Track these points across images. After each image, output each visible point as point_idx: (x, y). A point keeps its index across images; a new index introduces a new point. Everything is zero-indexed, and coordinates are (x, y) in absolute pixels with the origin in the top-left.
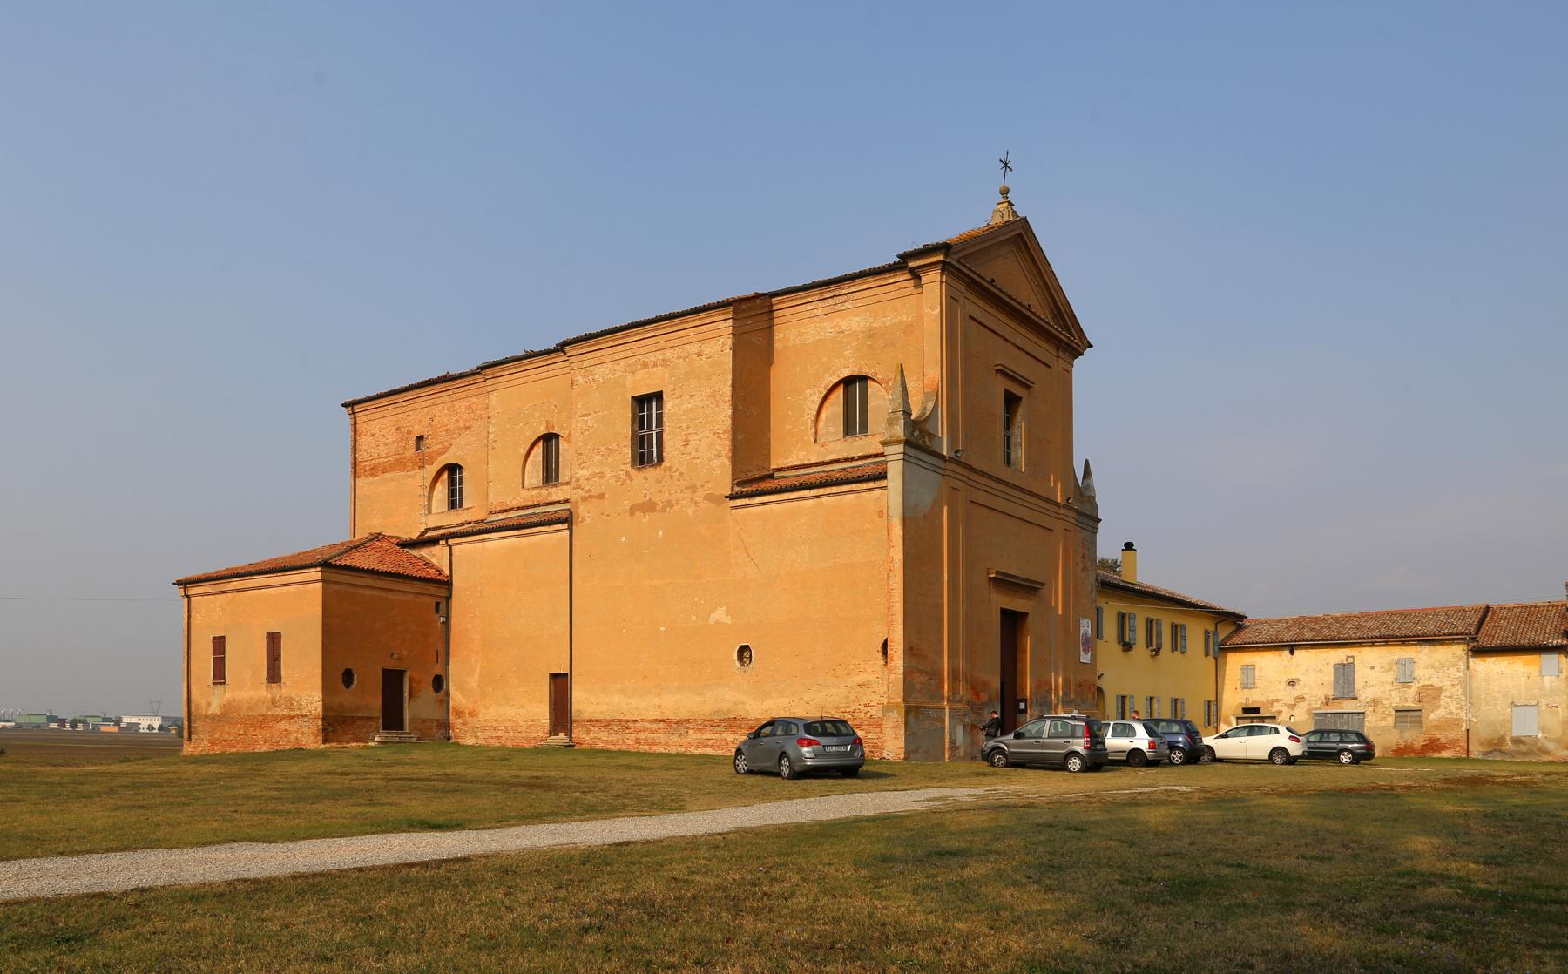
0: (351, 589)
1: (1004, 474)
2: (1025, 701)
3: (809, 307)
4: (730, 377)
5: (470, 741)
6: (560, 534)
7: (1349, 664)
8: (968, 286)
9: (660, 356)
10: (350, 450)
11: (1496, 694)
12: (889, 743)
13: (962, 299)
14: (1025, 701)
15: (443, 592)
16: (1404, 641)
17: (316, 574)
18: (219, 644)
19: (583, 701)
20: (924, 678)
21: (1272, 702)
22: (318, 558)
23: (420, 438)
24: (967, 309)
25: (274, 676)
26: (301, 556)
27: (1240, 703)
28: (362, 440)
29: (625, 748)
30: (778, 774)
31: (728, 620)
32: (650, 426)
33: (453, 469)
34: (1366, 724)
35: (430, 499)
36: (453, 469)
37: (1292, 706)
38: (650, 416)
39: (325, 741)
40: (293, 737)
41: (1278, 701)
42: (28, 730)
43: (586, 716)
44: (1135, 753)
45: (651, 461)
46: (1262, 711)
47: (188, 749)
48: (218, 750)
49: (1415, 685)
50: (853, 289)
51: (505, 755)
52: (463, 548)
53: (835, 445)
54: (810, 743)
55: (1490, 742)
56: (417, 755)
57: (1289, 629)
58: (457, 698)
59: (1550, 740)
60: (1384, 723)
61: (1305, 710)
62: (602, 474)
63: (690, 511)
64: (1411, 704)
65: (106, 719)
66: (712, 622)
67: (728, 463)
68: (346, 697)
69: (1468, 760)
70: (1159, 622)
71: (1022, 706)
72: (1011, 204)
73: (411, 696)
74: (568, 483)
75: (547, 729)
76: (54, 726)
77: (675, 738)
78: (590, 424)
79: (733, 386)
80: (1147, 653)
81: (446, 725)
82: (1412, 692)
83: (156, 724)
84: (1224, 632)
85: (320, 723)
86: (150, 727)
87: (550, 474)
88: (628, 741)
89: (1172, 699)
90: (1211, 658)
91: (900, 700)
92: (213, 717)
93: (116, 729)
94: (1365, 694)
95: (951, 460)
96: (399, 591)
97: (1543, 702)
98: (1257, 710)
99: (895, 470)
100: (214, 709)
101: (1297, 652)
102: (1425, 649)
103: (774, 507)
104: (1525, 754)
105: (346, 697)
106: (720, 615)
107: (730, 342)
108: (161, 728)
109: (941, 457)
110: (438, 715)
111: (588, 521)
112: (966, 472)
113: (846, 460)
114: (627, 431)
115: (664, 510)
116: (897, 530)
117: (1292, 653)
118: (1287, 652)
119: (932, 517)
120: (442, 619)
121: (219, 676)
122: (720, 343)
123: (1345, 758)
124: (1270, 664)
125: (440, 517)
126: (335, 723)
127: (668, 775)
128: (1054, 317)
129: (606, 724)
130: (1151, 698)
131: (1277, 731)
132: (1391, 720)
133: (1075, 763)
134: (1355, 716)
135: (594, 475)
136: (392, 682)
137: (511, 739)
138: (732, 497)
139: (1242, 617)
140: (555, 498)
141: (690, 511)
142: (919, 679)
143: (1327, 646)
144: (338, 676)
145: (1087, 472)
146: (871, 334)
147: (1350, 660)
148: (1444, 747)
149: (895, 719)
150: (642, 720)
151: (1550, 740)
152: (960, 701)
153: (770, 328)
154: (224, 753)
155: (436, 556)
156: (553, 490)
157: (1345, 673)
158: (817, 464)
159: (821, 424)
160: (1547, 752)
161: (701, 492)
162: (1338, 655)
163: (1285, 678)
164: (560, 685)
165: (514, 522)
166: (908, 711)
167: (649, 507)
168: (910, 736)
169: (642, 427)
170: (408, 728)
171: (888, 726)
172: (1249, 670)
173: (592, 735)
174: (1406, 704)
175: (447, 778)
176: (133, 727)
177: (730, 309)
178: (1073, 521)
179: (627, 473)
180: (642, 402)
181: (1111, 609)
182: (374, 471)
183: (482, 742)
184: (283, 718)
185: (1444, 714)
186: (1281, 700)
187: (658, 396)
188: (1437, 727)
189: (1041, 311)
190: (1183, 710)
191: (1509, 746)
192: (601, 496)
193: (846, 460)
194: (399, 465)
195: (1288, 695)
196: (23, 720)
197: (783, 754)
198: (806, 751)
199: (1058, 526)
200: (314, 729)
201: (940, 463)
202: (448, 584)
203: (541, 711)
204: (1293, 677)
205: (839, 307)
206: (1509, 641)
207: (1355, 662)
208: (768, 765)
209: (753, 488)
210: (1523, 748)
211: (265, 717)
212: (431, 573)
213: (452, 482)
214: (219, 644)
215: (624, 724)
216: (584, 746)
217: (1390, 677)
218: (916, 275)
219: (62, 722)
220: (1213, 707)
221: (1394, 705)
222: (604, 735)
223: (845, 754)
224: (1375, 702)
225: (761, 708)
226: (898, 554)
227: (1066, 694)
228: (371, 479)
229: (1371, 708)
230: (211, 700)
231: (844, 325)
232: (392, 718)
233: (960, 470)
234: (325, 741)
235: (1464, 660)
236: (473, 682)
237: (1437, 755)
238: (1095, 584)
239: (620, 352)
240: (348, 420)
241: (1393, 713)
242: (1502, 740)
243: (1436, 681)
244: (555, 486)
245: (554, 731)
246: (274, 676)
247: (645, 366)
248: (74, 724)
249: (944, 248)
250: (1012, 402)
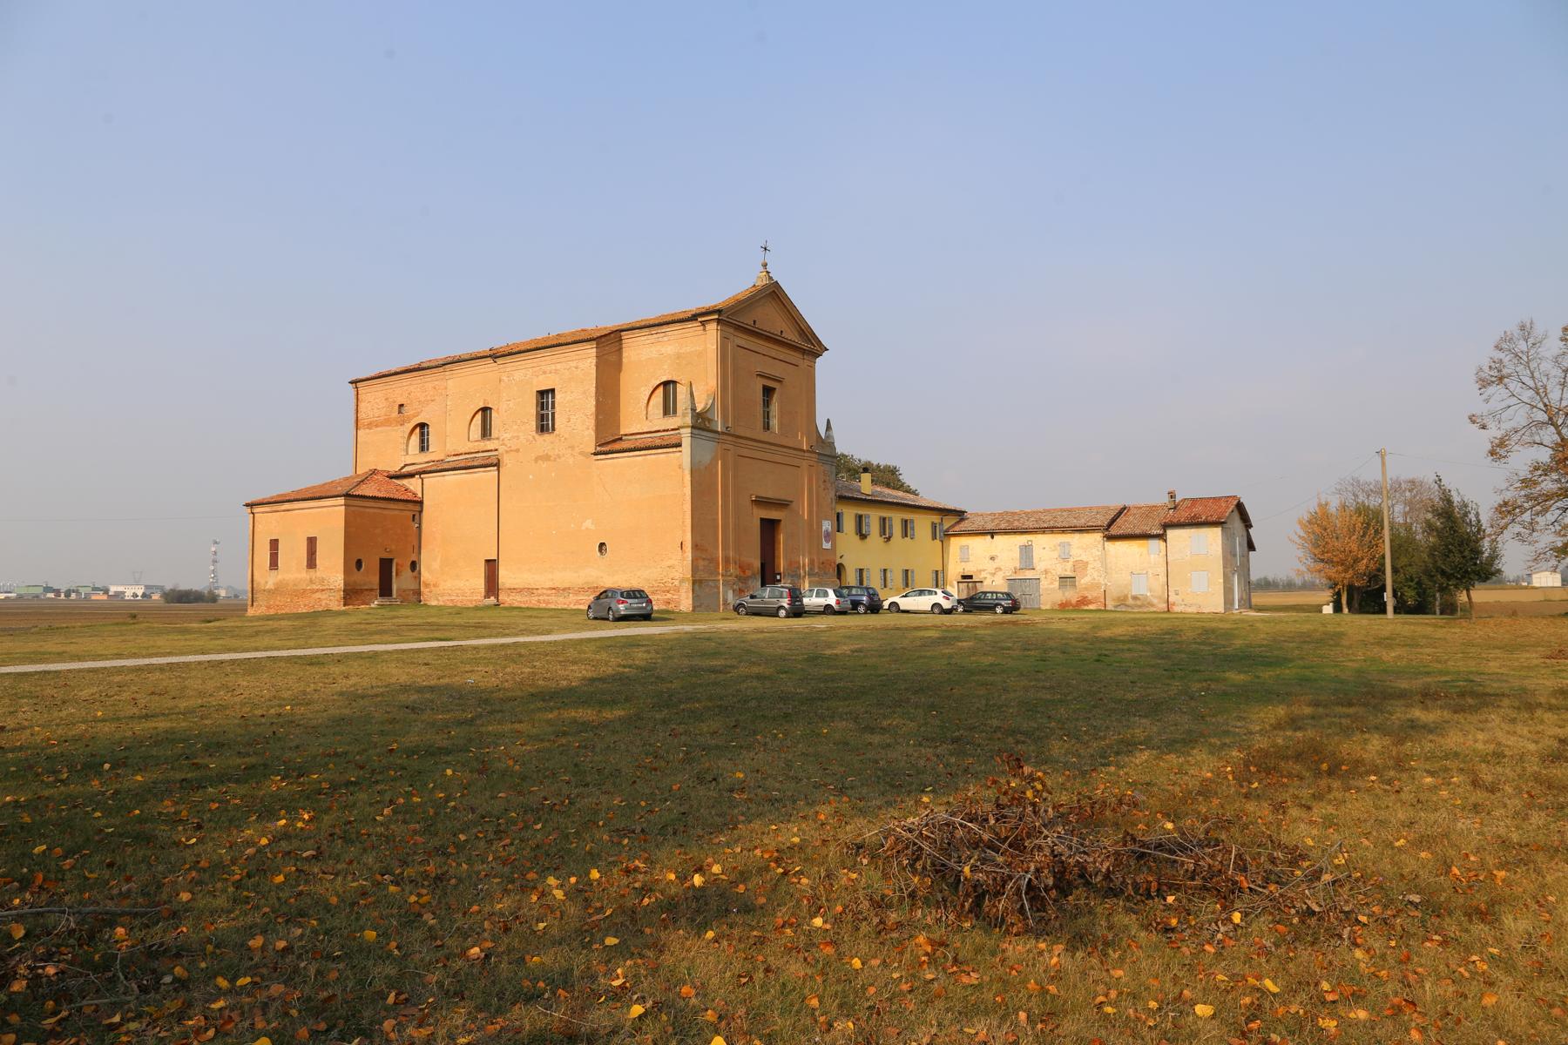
0: (362, 509)
1: (764, 436)
2: (780, 574)
3: (643, 338)
5: (434, 603)
6: (492, 473)
8: (736, 329)
9: (553, 367)
10: (354, 412)
12: (685, 603)
13: (732, 337)
14: (780, 574)
15: (418, 508)
16: (1064, 530)
17: (341, 501)
18: (274, 544)
19: (505, 577)
20: (706, 563)
21: (980, 571)
22: (340, 490)
23: (401, 406)
25: (311, 563)
26: (327, 487)
28: (361, 405)
29: (531, 606)
30: (608, 619)
31: (593, 527)
32: (547, 409)
35: (407, 446)
36: (422, 426)
38: (548, 402)
39: (345, 605)
40: (323, 603)
41: (984, 570)
42: (28, 600)
43: (508, 586)
44: (828, 607)
45: (548, 430)
47: (251, 612)
48: (272, 612)
49: (1072, 560)
51: (459, 611)
52: (430, 480)
53: (658, 421)
54: (623, 602)
55: (1119, 599)
56: (403, 612)
57: (993, 520)
58: (426, 575)
59: (1155, 597)
60: (1052, 586)
62: (518, 437)
63: (571, 461)
64: (1069, 574)
65: (95, 589)
66: (583, 528)
67: (593, 433)
68: (358, 577)
69: (1106, 611)
70: (890, 519)
71: (778, 577)
72: (768, 272)
73: (397, 574)
74: (498, 439)
75: (483, 594)
76: (51, 595)
77: (561, 599)
78: (511, 406)
79: (597, 387)
80: (882, 540)
81: (418, 593)
82: (1069, 566)
83: (140, 593)
84: (948, 522)
86: (135, 595)
87: (486, 432)
88: (533, 601)
90: (938, 542)
91: (690, 576)
92: (269, 591)
93: (105, 597)
95: (723, 433)
97: (1150, 572)
98: (971, 577)
99: (686, 442)
100: (270, 585)
102: (1077, 536)
104: (1140, 607)
105: (358, 577)
106: (588, 524)
108: (144, 595)
109: (717, 432)
110: (413, 586)
111: (509, 465)
112: (734, 439)
113: (664, 431)
115: (555, 459)
116: (688, 478)
117: (992, 537)
118: (989, 537)
119: (711, 468)
121: (274, 564)
123: (999, 610)
124: (978, 545)
125: (413, 456)
126: (351, 593)
127: (550, 620)
128: (800, 335)
129: (520, 591)
130: (885, 570)
131: (936, 593)
133: (782, 613)
134: (1034, 581)
135: (514, 437)
136: (386, 566)
137: (461, 601)
138: (595, 454)
139: (962, 513)
140: (489, 448)
141: (571, 461)
142: (701, 563)
143: (1006, 533)
144: (354, 564)
145: (829, 427)
146: (679, 356)
148: (1090, 602)
149: (688, 586)
151: (1155, 597)
152: (730, 576)
153: (620, 350)
154: (276, 614)
155: (413, 484)
156: (488, 442)
157: (1026, 551)
158: (647, 433)
159: (650, 408)
160: (1153, 605)
161: (577, 450)
163: (988, 555)
164: (492, 566)
165: (463, 465)
166: (694, 582)
167: (546, 458)
168: (696, 597)
169: (543, 420)
170: (394, 595)
171: (683, 591)
172: (965, 549)
175: (429, 624)
176: (119, 595)
177: (594, 342)
179: (534, 437)
180: (542, 394)
181: (849, 514)
182: (370, 426)
183: (441, 603)
184: (317, 591)
187: (553, 391)
188: (1086, 589)
189: (791, 336)
190: (913, 577)
191: (1130, 602)
192: (518, 450)
193: (664, 431)
194: (387, 422)
195: (991, 566)
196: (22, 592)
197: (610, 608)
198: (621, 607)
199: (805, 464)
200: (338, 597)
201: (716, 436)
202: (421, 503)
203: (480, 583)
204: (993, 554)
206: (1129, 531)
208: (603, 614)
210: (1139, 603)
211: (305, 591)
212: (410, 496)
213: (422, 434)
214: (274, 544)
215: (530, 591)
216: (506, 605)
217: (1056, 555)
218: (703, 324)
219: (58, 592)
220: (940, 575)
222: (518, 598)
223: (642, 608)
224: (1046, 572)
225: (609, 582)
226: (688, 491)
227: (811, 569)
228: (367, 431)
230: (268, 580)
231: (663, 350)
232: (385, 590)
233: (730, 438)
234: (345, 605)
236: (436, 565)
237: (1086, 608)
238: (834, 497)
239: (529, 363)
240: (353, 392)
242: (1126, 597)
243: (1084, 558)
244: (489, 440)
245: (487, 596)
246: (311, 563)
247: (545, 373)
248: (68, 594)
249: (719, 312)
250: (768, 392)
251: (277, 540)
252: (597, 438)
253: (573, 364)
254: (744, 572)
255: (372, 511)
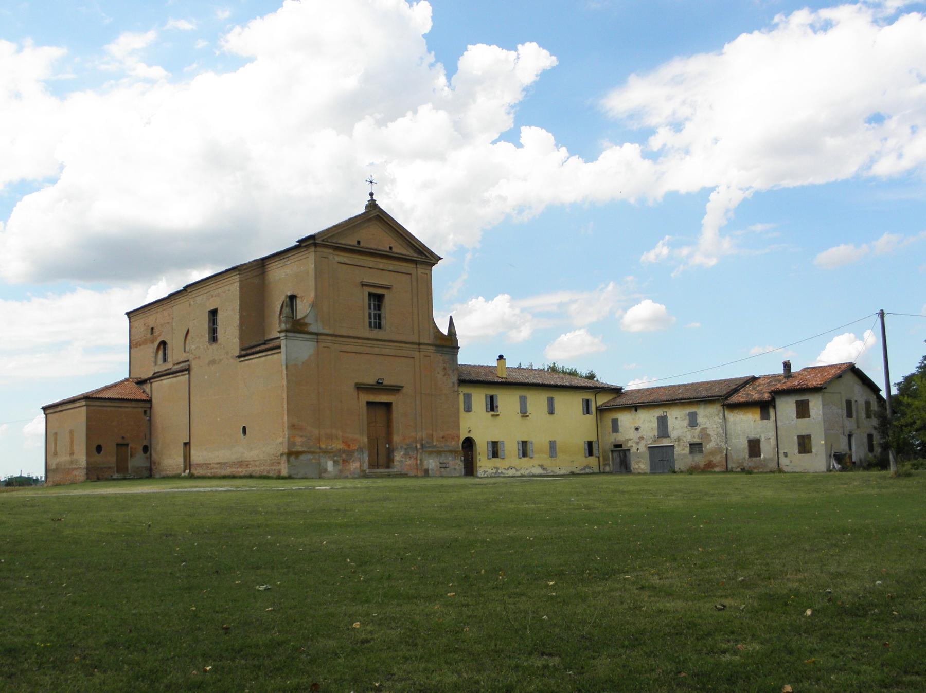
3: (276, 263)
4: (238, 301)
7: (665, 416)
11: (739, 432)
15: (148, 405)
17: (83, 403)
21: (628, 440)
24: (336, 259)
27: (612, 442)
33: (164, 344)
34: (675, 452)
37: (638, 443)
41: (630, 440)
46: (623, 446)
50: (290, 255)
60: (683, 452)
61: (644, 445)
64: (697, 440)
67: (238, 341)
68: (98, 458)
85: (85, 470)
89: (488, 443)
94: (674, 434)
96: (125, 407)
101: (639, 411)
103: (253, 361)
107: (238, 284)
111: (195, 369)
114: (206, 327)
120: (148, 418)
122: (236, 285)
132: (687, 450)
138: (239, 357)
147: (665, 414)
150: (213, 463)
157: (663, 422)
162: (658, 412)
163: (633, 426)
173: (197, 471)
174: (695, 440)
178: (433, 351)
179: (207, 347)
185: (714, 445)
186: (632, 439)
189: (400, 249)
202: (150, 401)
204: (637, 426)
205: (286, 263)
207: (668, 415)
209: (249, 351)
221: (688, 440)
224: (679, 439)
229: (677, 443)
235: (722, 412)
240: (127, 320)
241: (688, 445)
247: (212, 297)
251: (809, 437)
252: (240, 346)
253: (227, 288)
254: (349, 446)
255: (108, 409)
